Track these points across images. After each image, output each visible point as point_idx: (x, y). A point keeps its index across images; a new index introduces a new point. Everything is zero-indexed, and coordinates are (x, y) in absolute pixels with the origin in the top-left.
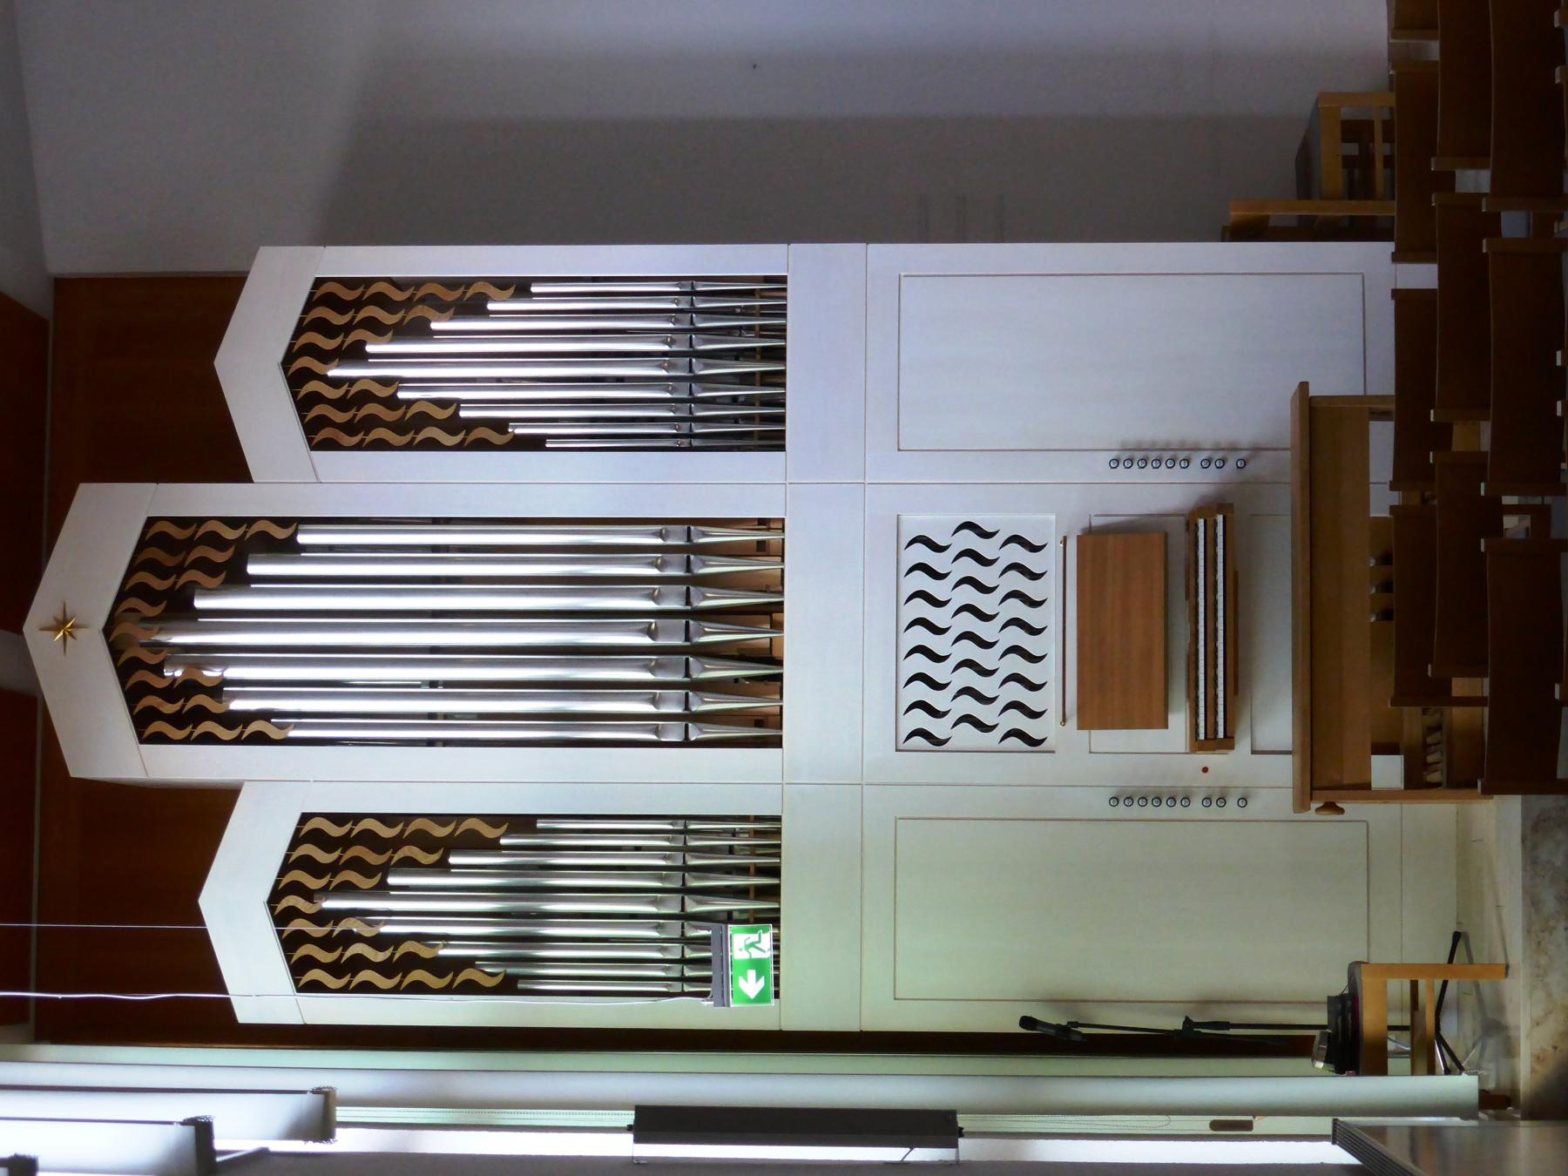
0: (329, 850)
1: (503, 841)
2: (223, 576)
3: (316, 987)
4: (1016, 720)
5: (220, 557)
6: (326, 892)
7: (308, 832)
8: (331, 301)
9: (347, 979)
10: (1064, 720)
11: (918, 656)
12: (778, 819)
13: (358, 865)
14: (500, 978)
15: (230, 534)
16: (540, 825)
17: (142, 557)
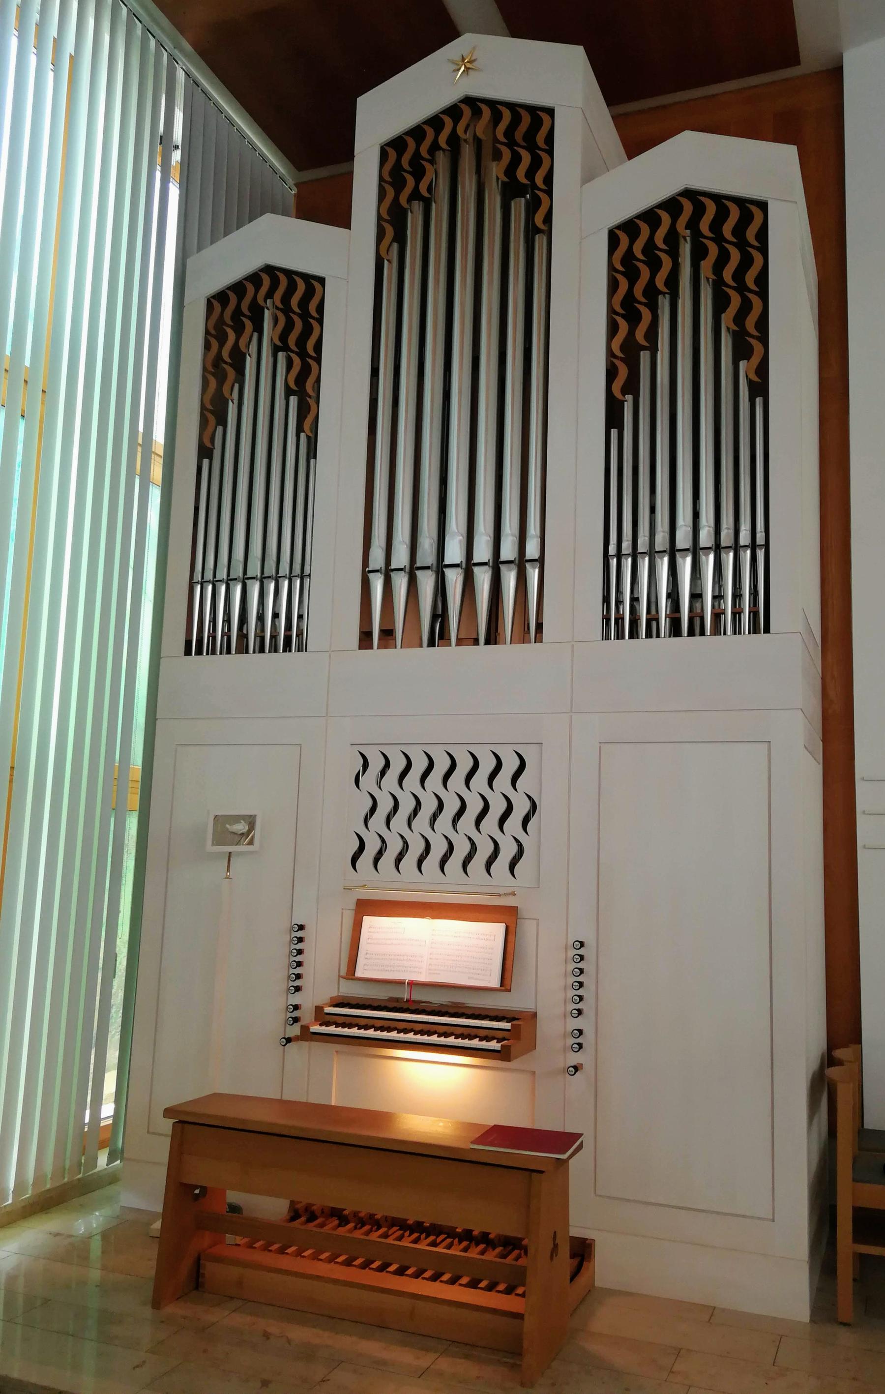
0: (734, 232)
1: (302, 435)
5: (521, 174)
6: (696, 235)
7: (314, 284)
9: (621, 268)
12: (767, 630)
13: (289, 326)
14: (209, 445)
17: (523, 112)
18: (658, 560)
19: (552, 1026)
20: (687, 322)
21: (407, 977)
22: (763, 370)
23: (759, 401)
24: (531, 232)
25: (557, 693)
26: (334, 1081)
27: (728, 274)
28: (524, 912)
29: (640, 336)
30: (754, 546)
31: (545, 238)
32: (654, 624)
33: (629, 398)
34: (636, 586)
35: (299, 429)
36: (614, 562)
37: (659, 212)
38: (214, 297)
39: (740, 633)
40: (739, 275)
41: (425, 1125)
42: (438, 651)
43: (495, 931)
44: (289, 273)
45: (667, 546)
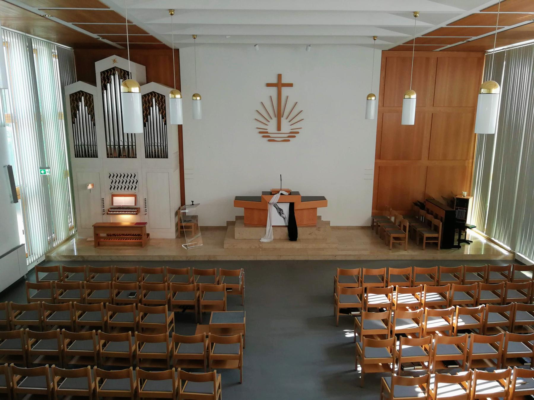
4: (113, 187)
19: (142, 209)
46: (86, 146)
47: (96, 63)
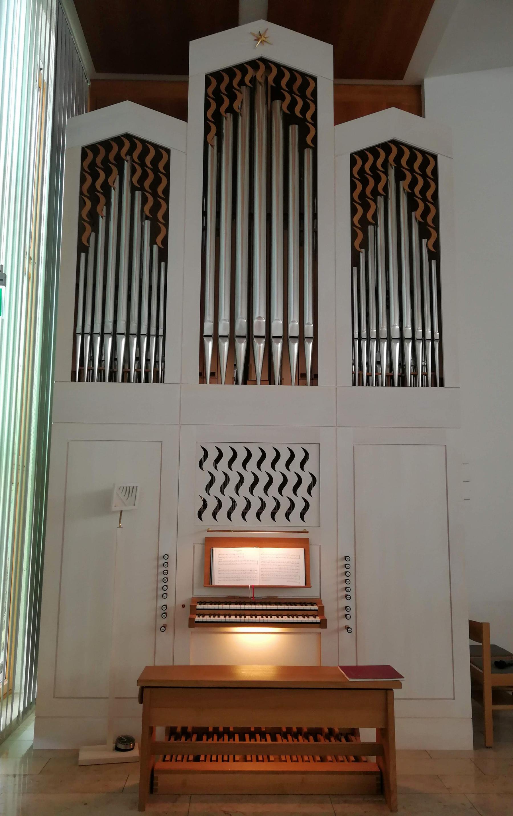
0: (152, 163)
1: (155, 247)
2: (288, 112)
3: (353, 162)
4: (212, 505)
7: (162, 153)
8: (425, 163)
10: (208, 531)
11: (274, 454)
14: (86, 244)
15: (309, 115)
16: (163, 264)
17: (297, 75)
18: (381, 343)
20: (394, 215)
21: (250, 583)
22: (437, 244)
23: (434, 262)
24: (302, 145)
25: (316, 416)
26: (196, 652)
27: (417, 190)
28: (311, 542)
29: (369, 216)
30: (360, 339)
31: (311, 151)
32: (370, 378)
33: (363, 250)
34: (149, 353)
35: (153, 242)
36: (357, 342)
37: (379, 149)
38: (88, 147)
39: (416, 386)
40: (423, 191)
41: (251, 672)
42: (249, 387)
43: (300, 552)
44: (144, 142)
45: (244, 332)
46: (260, 347)
47: (190, 42)
